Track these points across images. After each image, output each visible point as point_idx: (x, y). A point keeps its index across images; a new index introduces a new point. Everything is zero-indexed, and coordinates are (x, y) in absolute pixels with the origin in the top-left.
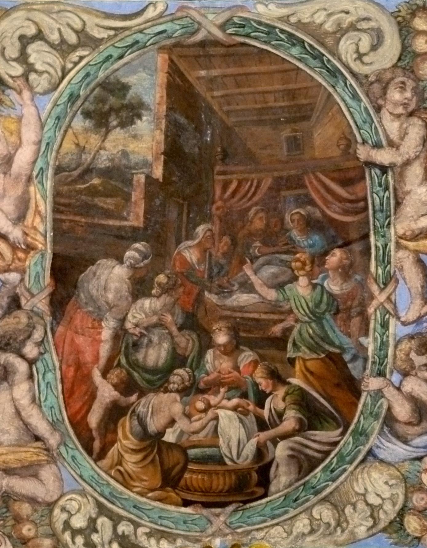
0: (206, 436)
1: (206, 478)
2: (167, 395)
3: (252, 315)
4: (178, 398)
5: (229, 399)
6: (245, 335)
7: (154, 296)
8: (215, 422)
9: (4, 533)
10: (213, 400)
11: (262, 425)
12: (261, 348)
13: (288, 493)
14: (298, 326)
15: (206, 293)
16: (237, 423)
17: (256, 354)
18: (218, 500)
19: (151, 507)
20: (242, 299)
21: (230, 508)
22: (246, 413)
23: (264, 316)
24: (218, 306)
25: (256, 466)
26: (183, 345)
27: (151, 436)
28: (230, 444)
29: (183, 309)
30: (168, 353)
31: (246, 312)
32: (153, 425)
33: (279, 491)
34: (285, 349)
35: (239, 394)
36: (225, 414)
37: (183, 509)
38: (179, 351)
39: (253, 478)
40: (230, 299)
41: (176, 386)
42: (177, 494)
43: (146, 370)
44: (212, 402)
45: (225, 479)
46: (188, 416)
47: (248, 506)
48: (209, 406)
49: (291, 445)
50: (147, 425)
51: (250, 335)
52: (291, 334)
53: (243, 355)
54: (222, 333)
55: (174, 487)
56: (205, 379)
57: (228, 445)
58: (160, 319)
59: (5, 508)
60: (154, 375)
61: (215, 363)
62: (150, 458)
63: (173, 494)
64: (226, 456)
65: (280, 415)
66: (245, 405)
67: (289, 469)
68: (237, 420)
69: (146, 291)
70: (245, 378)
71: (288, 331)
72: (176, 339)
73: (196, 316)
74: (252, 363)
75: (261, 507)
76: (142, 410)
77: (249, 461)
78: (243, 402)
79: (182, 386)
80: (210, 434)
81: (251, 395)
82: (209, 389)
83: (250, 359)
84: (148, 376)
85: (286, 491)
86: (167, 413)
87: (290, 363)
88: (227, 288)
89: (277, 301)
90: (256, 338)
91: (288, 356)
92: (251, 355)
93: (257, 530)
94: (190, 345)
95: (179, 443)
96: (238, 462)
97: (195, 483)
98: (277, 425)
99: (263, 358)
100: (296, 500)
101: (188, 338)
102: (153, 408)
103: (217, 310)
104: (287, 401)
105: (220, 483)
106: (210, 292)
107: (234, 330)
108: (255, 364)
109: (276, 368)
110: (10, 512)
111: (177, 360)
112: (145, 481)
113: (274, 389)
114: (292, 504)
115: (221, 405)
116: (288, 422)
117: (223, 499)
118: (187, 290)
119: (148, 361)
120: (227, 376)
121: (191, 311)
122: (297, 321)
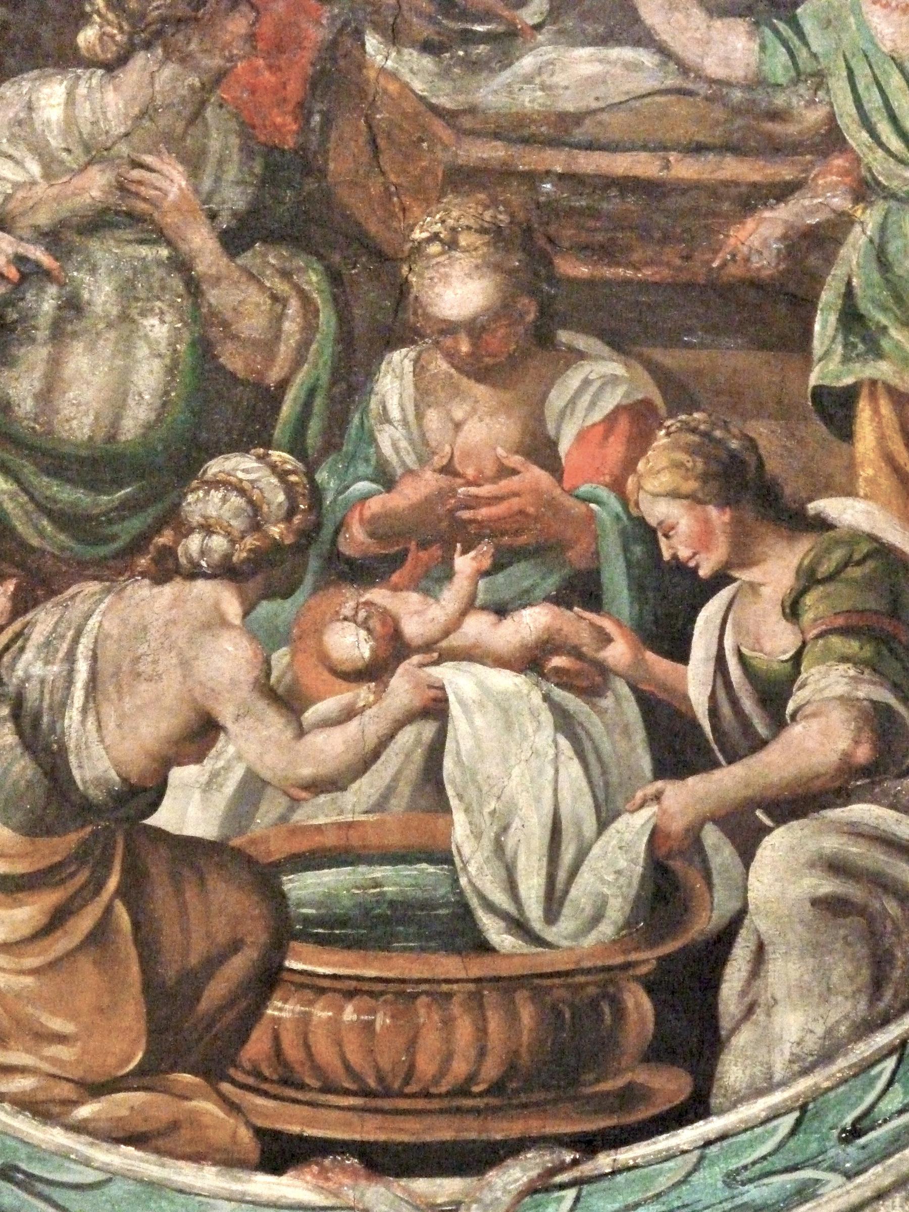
0: (380, 805)
1: (382, 1020)
2: (168, 590)
3: (621, 164)
4: (232, 607)
5: (501, 611)
6: (584, 271)
7: (91, 63)
8: (428, 729)
10: (418, 615)
11: (678, 746)
12: (672, 340)
13: (818, 1094)
14: (869, 219)
15: (372, 42)
16: (544, 735)
17: (645, 376)
18: (443, 1131)
19: (91, 1176)
20: (570, 72)
21: (513, 1176)
22: (590, 680)
23: (686, 169)
24: (435, 110)
25: (647, 958)
26: (252, 325)
27: (85, 809)
28: (510, 842)
29: (246, 130)
30: (171, 370)
31: (591, 146)
32: (97, 750)
33: (770, 1087)
34: (799, 342)
35: (551, 584)
36: (480, 684)
37: (264, 1185)
38: (233, 359)
39: (633, 1017)
40: (505, 76)
41: (218, 543)
42: (233, 1107)
43: (60, 462)
44: (413, 630)
45: (482, 1031)
46: (289, 701)
47: (604, 1161)
48: (394, 649)
49: (831, 844)
50: (63, 750)
51: (608, 272)
52: (830, 261)
53: (574, 379)
54: (462, 263)
55: (214, 1070)
56: (374, 505)
57: (499, 848)
58: (122, 188)
60: (94, 486)
61: (424, 423)
62: (84, 922)
63: (207, 1107)
64: (491, 907)
65: (774, 693)
66: (584, 638)
67: (822, 972)
68: (546, 717)
69: (46, 33)
70: (586, 500)
71: (816, 243)
72: (213, 296)
73: (323, 172)
74: (623, 424)
75: (675, 1169)
76: (37, 670)
77: (606, 930)
78: (575, 624)
79: (250, 542)
80: (405, 789)
81: (616, 580)
82: (397, 561)
83: (611, 400)
84: (67, 495)
85: (803, 1085)
86: (171, 687)
87: (828, 419)
88: (486, 16)
89: (758, 82)
90: (644, 286)
91: (814, 379)
92: (614, 380)
94: (291, 326)
95: (235, 842)
96: (550, 934)
97: (325, 1052)
98: (759, 745)
99: (679, 393)
100: (855, 1132)
101: (281, 287)
102: (94, 658)
103: (434, 139)
104: (808, 617)
105: (457, 1045)
106: (394, 36)
107: (525, 248)
108: (639, 422)
109: (752, 444)
111: (221, 405)
112: (61, 1039)
113: (742, 554)
114: (835, 1152)
115: (455, 640)
116: (815, 725)
117: (471, 1131)
118: (266, 28)
119: (67, 411)
120: (485, 490)
121: (290, 143)
122: (865, 189)
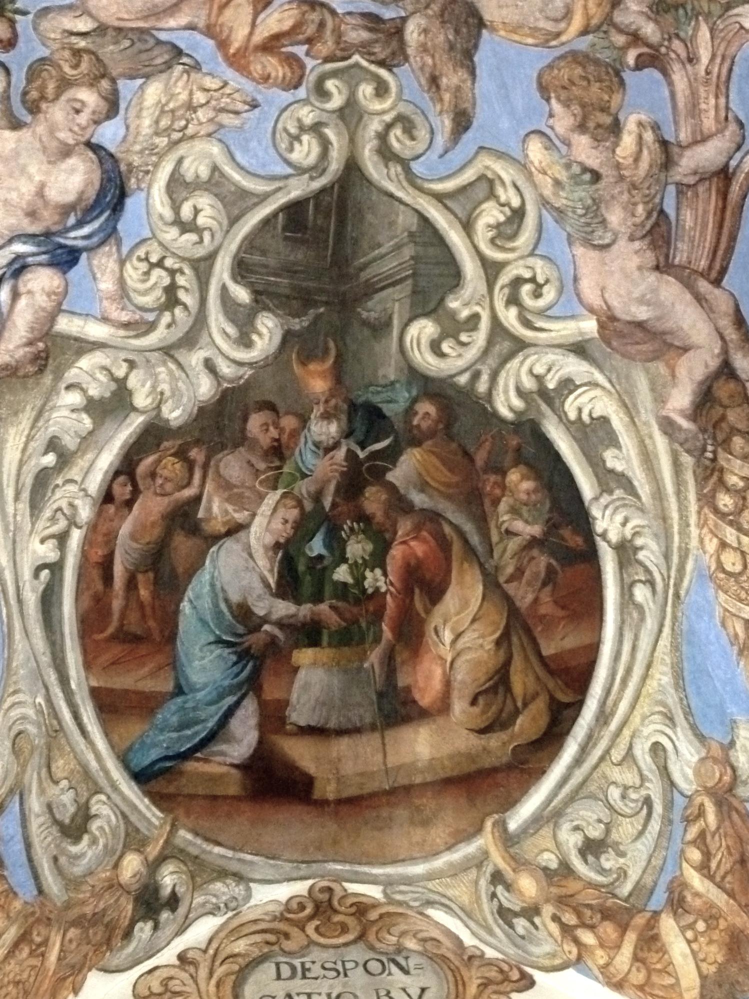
9: (720, 17)
30: (419, 726)
59: (677, 10)
93: (645, 677)
110: (686, 3)
